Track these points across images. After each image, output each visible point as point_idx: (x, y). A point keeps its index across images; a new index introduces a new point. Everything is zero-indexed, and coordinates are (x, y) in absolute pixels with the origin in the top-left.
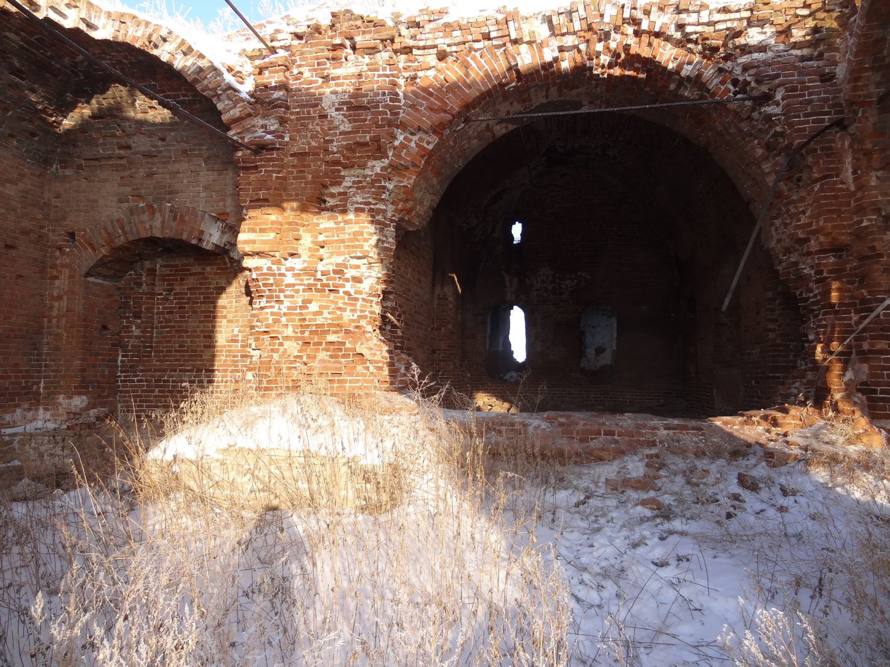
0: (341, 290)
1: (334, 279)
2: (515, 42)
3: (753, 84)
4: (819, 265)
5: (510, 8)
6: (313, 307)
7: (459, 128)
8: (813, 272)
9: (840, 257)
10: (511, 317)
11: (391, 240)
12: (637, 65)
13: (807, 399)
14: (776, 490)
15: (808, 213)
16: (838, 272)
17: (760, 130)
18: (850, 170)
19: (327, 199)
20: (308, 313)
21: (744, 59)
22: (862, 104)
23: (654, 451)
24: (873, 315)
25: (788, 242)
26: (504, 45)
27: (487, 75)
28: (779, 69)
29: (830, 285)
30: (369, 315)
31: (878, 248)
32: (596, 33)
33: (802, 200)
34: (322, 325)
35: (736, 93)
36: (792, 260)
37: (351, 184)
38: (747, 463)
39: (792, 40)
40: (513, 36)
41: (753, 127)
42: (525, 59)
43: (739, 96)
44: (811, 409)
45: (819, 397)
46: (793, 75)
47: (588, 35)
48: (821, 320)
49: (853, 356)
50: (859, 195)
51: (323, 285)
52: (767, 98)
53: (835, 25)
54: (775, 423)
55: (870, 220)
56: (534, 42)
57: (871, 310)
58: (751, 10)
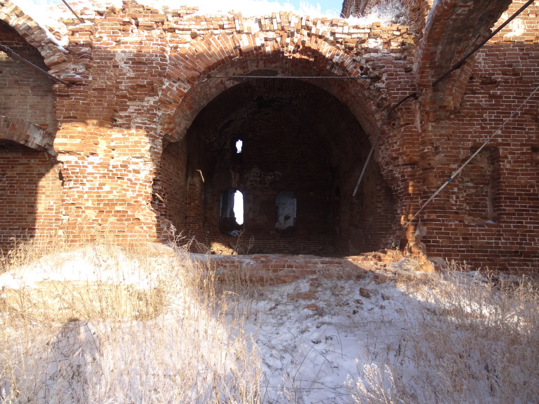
0: (126, 178)
2: (239, 32)
3: (371, 70)
4: (403, 172)
5: (236, 12)
6: (106, 188)
7: (204, 81)
8: (400, 176)
9: (414, 168)
10: (235, 197)
11: (159, 147)
12: (309, 53)
13: (396, 246)
14: (379, 297)
15: (398, 143)
16: (412, 176)
17: (374, 96)
18: (419, 121)
19: (118, 119)
21: (366, 56)
22: (425, 86)
23: (314, 277)
24: (429, 200)
25: (388, 159)
26: (232, 33)
27: (222, 50)
28: (384, 63)
29: (408, 183)
32: (286, 32)
33: (395, 136)
34: (112, 200)
35: (362, 74)
36: (390, 169)
37: (133, 111)
38: (365, 282)
39: (391, 48)
40: (238, 29)
41: (371, 94)
42: (245, 43)
43: (363, 76)
44: (398, 252)
45: (402, 245)
46: (391, 67)
47: (282, 33)
48: (404, 202)
49: (419, 222)
50: (423, 135)
52: (377, 79)
53: (412, 42)
54: (380, 259)
55: (428, 149)
56: (250, 33)
57: (428, 197)
58: (370, 29)
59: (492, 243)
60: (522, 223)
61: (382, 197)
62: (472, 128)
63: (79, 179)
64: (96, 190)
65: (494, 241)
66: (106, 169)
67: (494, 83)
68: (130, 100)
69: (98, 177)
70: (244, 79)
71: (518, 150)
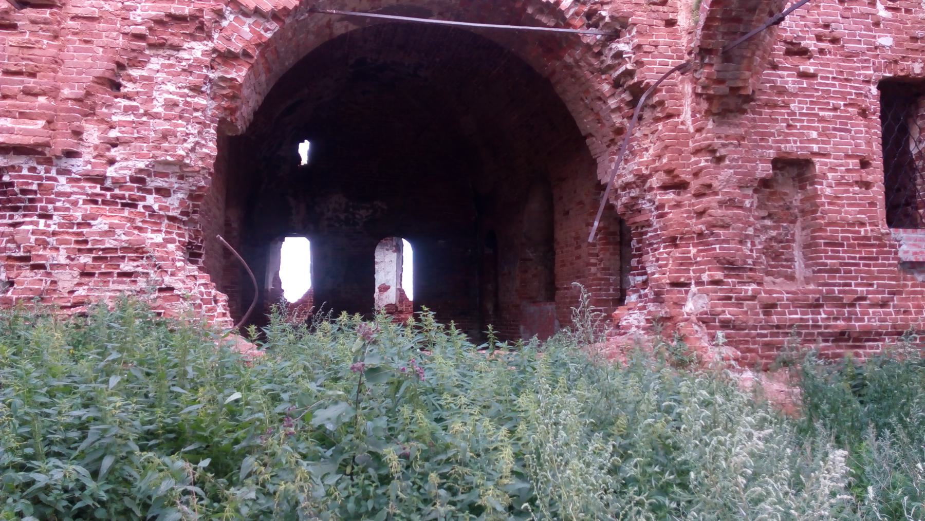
0: (141, 204)
1: (131, 189)
6: (100, 224)
7: (302, 18)
10: (282, 250)
11: (211, 144)
18: (690, 113)
19: (124, 83)
20: (93, 233)
30: (177, 238)
31: (714, 185)
34: (114, 250)
36: (632, 195)
37: (158, 67)
51: (114, 197)
59: (807, 320)
60: (850, 285)
61: (598, 247)
62: (774, 127)
63: (39, 205)
64: (75, 229)
65: (810, 316)
66: (99, 186)
67: (804, 53)
68: (151, 46)
69: (81, 202)
70: (368, 20)
71: (841, 165)
